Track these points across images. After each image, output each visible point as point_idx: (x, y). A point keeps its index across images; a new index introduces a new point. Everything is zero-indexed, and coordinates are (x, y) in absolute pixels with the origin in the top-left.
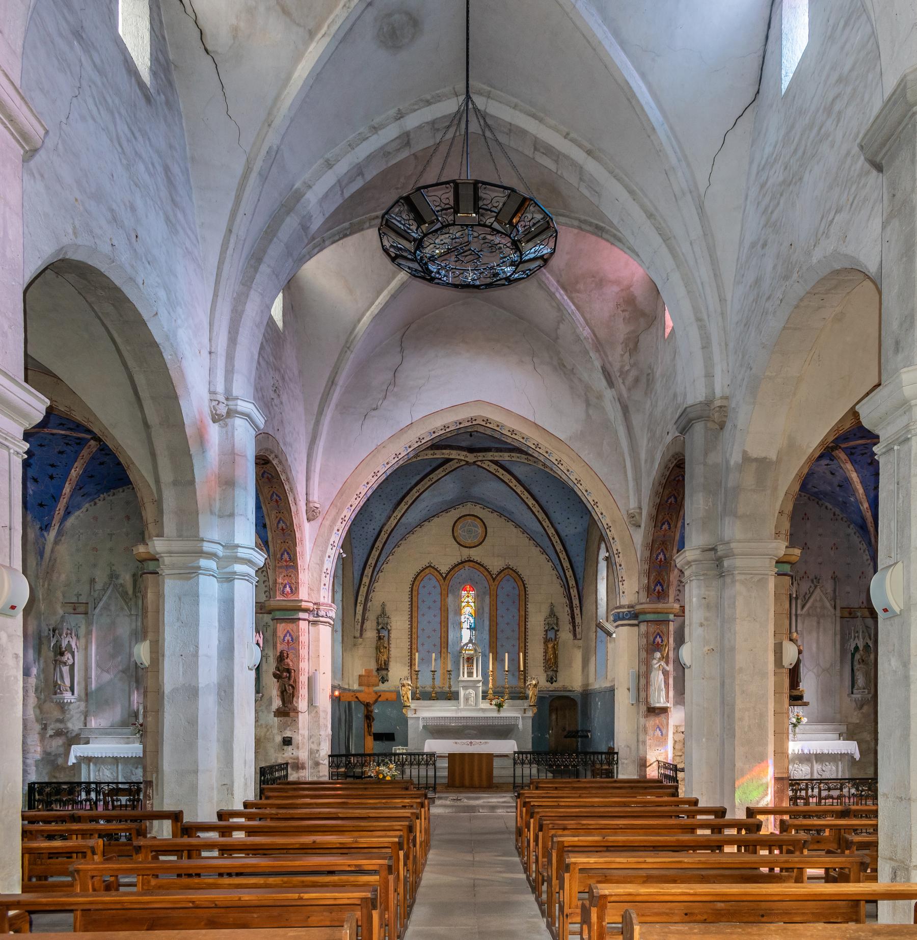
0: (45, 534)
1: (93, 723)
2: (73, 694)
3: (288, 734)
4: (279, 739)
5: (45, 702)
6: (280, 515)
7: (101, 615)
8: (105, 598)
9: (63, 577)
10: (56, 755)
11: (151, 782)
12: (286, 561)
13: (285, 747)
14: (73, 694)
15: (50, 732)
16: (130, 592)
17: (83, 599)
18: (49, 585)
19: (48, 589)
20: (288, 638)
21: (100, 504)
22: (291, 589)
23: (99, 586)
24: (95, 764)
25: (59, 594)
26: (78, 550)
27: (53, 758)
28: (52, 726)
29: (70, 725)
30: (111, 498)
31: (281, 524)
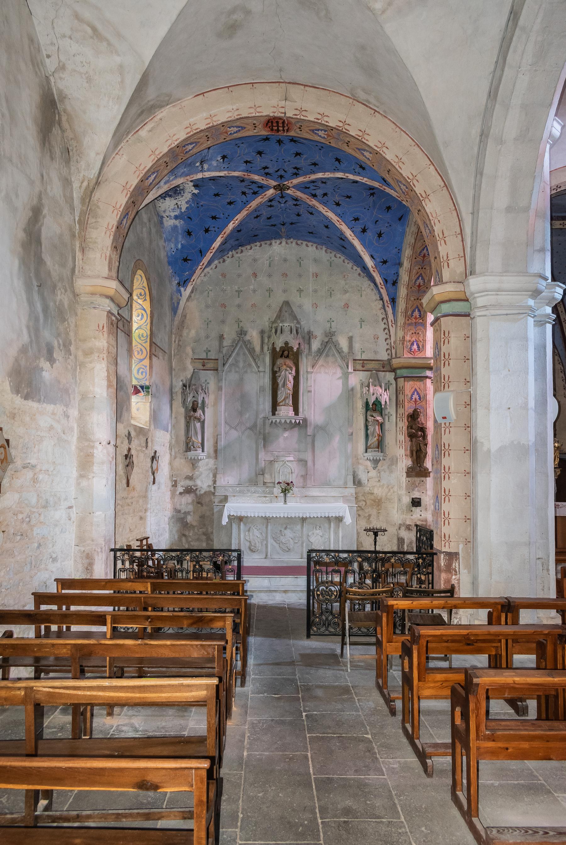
0: (182, 289)
1: (222, 481)
2: (203, 451)
3: (416, 495)
4: (407, 500)
5: (175, 458)
6: (421, 271)
7: (230, 371)
8: (234, 354)
9: (193, 333)
10: (185, 513)
11: (457, 554)
12: (416, 318)
13: (414, 509)
14: (203, 451)
15: (180, 489)
16: (258, 349)
17: (212, 355)
18: (179, 341)
19: (179, 345)
20: (416, 396)
21: (228, 261)
22: (418, 347)
23: (227, 343)
24: (245, 524)
25: (189, 350)
26: (207, 306)
27: (183, 516)
28: (182, 483)
29: (199, 483)
30: (239, 255)
31: (420, 281)
